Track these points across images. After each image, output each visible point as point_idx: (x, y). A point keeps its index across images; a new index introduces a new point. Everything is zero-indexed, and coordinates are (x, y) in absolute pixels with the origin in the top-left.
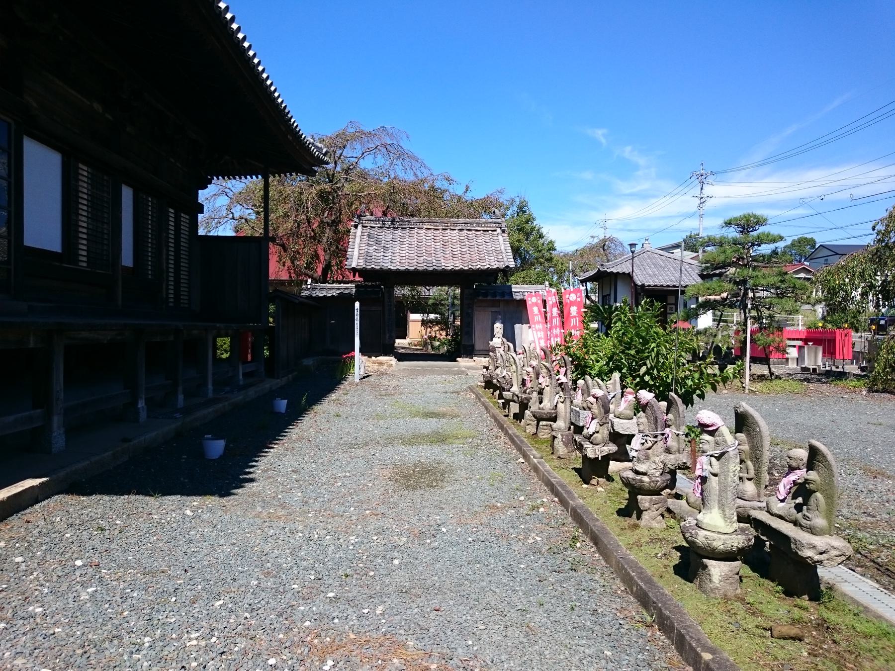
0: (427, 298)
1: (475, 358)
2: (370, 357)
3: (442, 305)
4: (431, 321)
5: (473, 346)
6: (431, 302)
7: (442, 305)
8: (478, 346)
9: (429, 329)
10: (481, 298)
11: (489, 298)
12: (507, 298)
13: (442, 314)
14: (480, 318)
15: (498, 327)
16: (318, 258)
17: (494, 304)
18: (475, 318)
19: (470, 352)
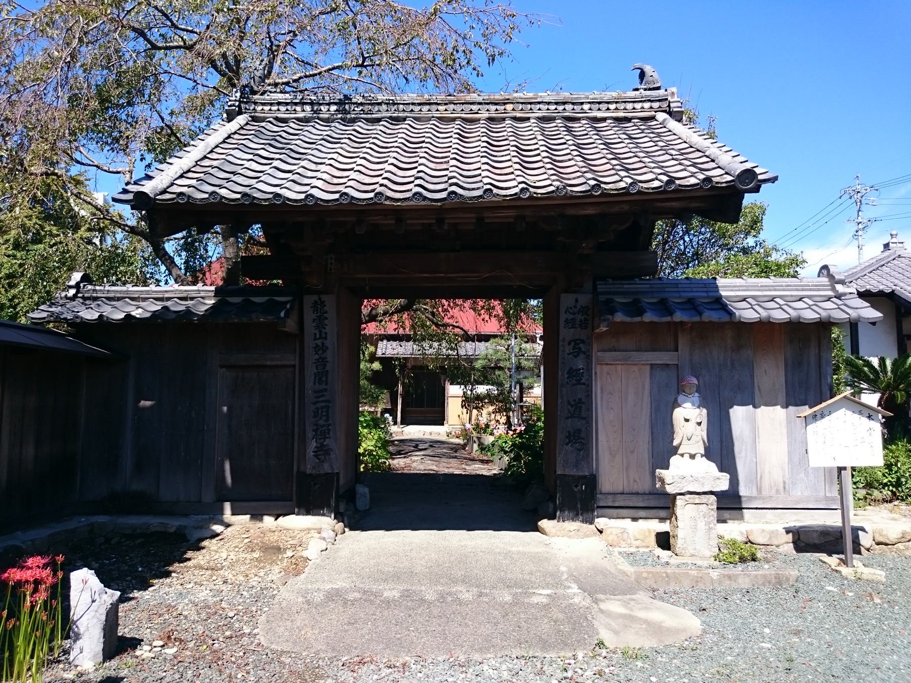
0: (470, 360)
1: (601, 522)
2: (257, 516)
3: (501, 368)
4: (479, 398)
5: (592, 481)
6: (478, 364)
7: (501, 368)
8: (612, 474)
9: (475, 412)
10: (619, 317)
11: (648, 317)
12: (710, 316)
13: (499, 384)
14: (618, 391)
15: (689, 420)
16: (128, 266)
17: (661, 336)
18: (597, 388)
19: (582, 500)
